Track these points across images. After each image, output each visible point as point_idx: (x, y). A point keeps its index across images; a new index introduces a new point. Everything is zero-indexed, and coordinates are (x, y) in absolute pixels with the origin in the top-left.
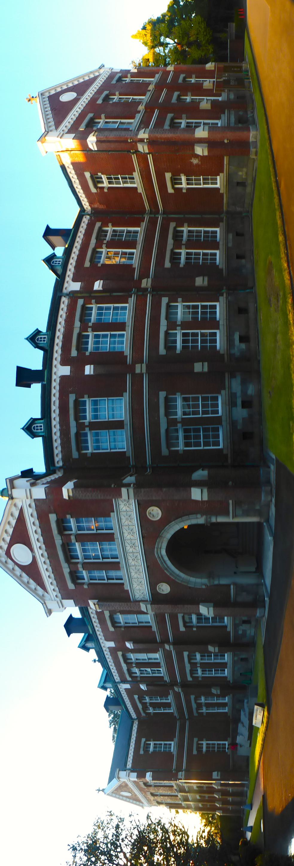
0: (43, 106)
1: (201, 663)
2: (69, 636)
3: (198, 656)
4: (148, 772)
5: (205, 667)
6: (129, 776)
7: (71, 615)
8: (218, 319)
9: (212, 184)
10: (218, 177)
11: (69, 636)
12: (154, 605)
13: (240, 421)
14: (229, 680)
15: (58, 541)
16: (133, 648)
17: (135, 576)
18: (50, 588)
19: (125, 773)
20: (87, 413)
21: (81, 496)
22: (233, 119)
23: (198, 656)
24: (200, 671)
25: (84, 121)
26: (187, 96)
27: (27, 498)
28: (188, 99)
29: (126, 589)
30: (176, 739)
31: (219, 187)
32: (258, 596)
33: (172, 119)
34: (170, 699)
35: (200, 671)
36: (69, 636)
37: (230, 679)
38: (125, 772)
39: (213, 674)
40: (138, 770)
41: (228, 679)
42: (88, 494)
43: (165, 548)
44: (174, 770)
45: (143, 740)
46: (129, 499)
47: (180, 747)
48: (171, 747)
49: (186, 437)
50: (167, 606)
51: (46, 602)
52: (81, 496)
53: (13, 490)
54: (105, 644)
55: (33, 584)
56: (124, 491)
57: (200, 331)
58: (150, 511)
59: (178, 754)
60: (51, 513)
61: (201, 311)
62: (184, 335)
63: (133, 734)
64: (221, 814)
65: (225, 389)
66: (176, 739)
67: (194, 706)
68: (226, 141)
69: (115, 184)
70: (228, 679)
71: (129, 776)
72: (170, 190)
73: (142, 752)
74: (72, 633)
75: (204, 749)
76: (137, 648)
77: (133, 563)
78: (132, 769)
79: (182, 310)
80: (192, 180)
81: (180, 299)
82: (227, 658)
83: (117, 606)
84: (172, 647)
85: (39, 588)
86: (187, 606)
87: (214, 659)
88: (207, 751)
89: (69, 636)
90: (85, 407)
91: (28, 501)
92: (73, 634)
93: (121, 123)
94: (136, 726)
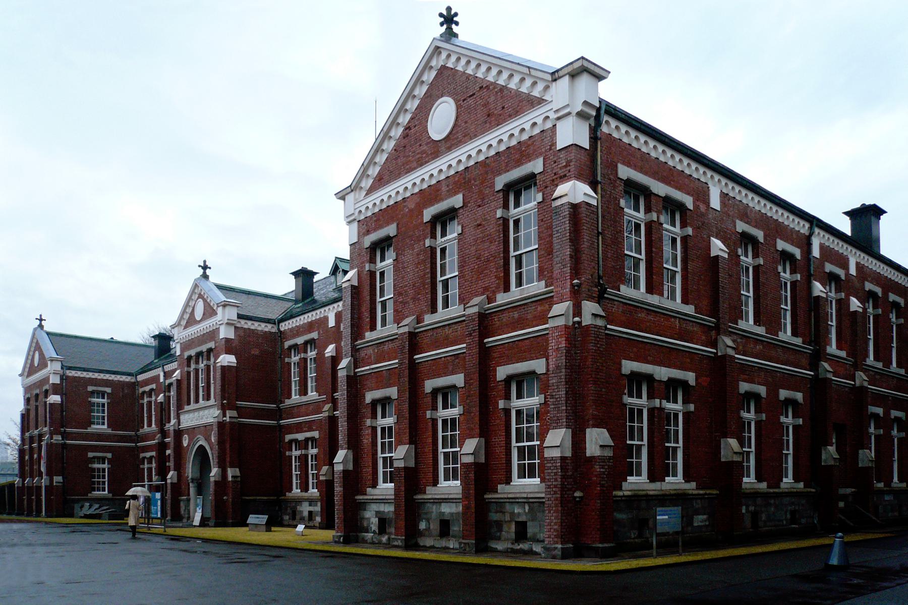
0: (458, 53)
1: (306, 456)
2: (847, 213)
3: (314, 451)
4: (62, 398)
5: (303, 459)
6: (54, 373)
7: (884, 212)
8: (93, 492)
9: (446, 470)
10: (537, 480)
11: (847, 213)
14: (368, 493)
15: (660, 188)
16: (327, 355)
19: (59, 368)
22: (446, 509)
23: (314, 451)
24: (298, 453)
26: (755, 413)
28: (750, 415)
30: (110, 431)
31: (511, 483)
33: (684, 384)
34: (312, 395)
35: (298, 453)
37: (431, 492)
38: (60, 369)
39: (295, 473)
40: (64, 384)
41: (430, 489)
44: (65, 430)
45: (109, 390)
47: (100, 437)
54: (332, 311)
55: (374, 171)
57: (644, 445)
59: (87, 434)
61: (633, 445)
62: (104, 470)
63: (106, 375)
64: (16, 486)
65: (113, 496)
66: (110, 431)
67: (301, 436)
69: (521, 269)
70: (430, 489)
71: (54, 373)
72: (90, 455)
73: (90, 389)
74: (851, 219)
75: (96, 466)
76: (217, 368)
78: (64, 377)
79: (672, 412)
80: (390, 437)
81: (110, 466)
82: (313, 492)
84: (326, 414)
85: (370, 181)
87: (313, 474)
88: (93, 470)
92: (850, 221)
93: (637, 262)
94: (127, 380)
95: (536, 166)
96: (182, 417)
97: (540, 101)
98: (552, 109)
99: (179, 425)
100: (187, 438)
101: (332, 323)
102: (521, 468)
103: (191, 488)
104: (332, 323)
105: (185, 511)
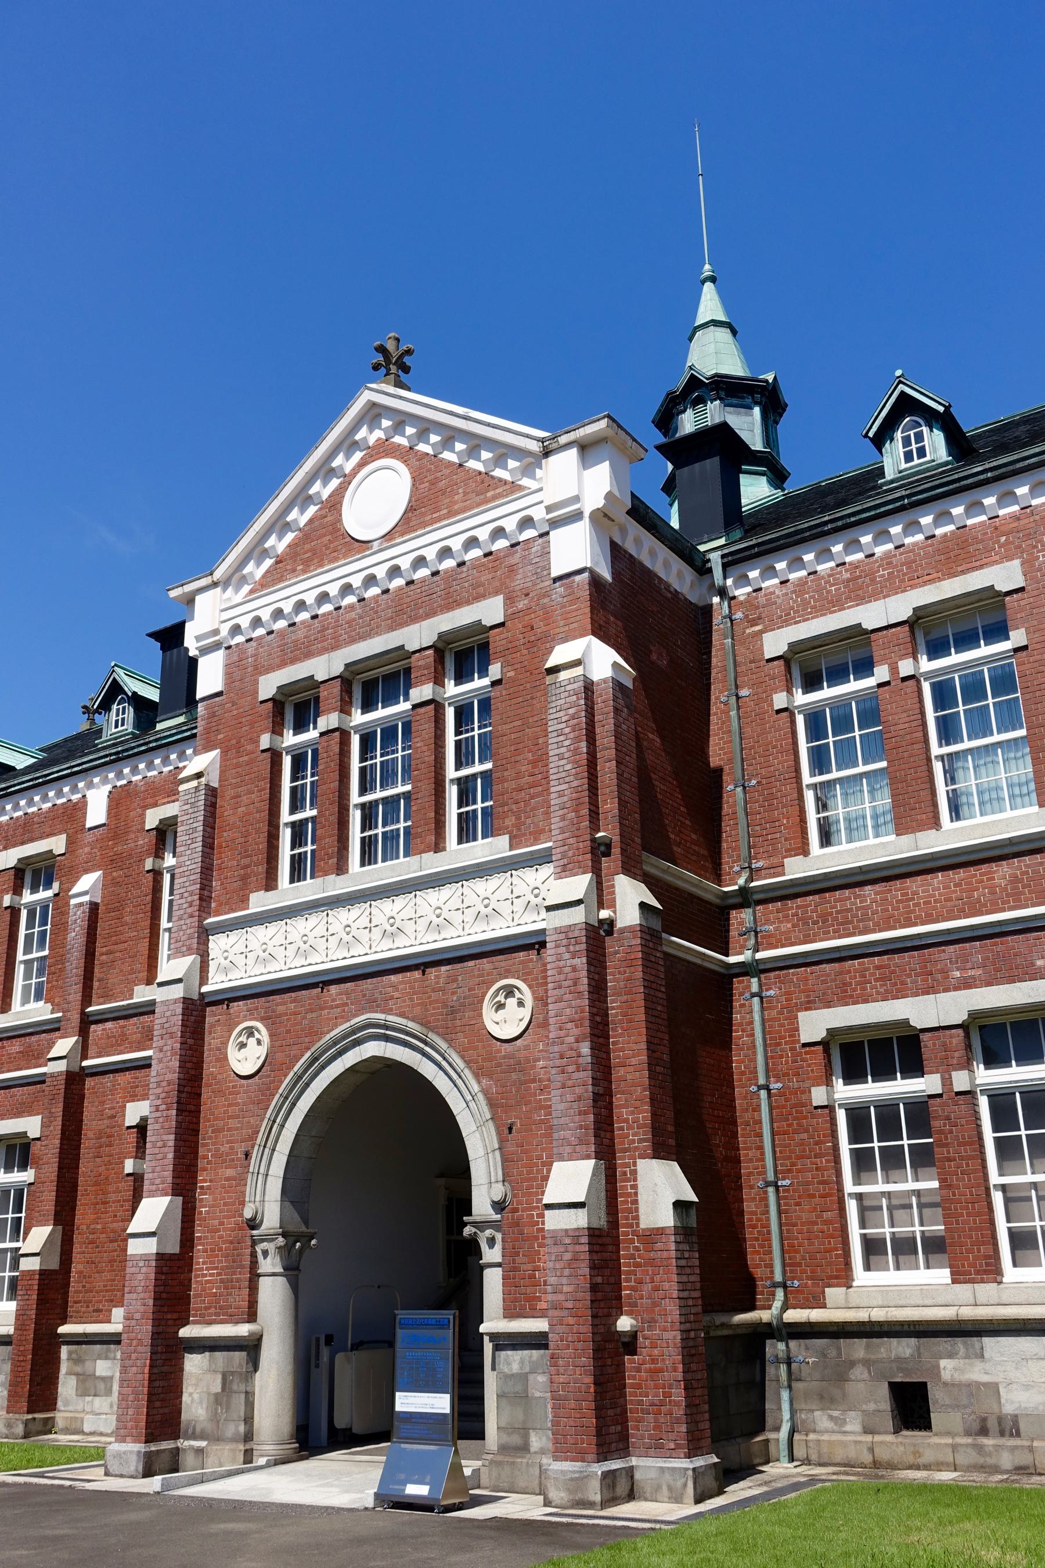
12: (179, 1011)
13: (977, 1373)
17: (336, 927)
18: (285, 597)
20: (805, 750)
21: (558, 715)
25: (499, 1296)
27: (549, 509)
29: (254, 897)
32: (203, 1444)
36: (150, 635)
42: (567, 743)
43: (387, 1056)
46: (549, 909)
48: (948, 755)
49: (887, 1111)
50: (176, 1064)
51: (219, 589)
52: (558, 715)
53: (573, 453)
56: (579, 885)
58: (518, 989)
60: (509, 601)
68: (624, 1323)
77: (336, 927)
83: (188, 863)
84: (61, 1066)
86: (171, 1143)
89: (150, 635)
90: (812, 747)
91: (539, 514)
95: (57, 844)
96: (217, 944)
97: (513, 488)
98: (542, 502)
99: (204, 980)
100: (264, 1034)
101: (97, 813)
102: (873, 1247)
103: (264, 1283)
104: (97, 813)
105: (220, 1400)
